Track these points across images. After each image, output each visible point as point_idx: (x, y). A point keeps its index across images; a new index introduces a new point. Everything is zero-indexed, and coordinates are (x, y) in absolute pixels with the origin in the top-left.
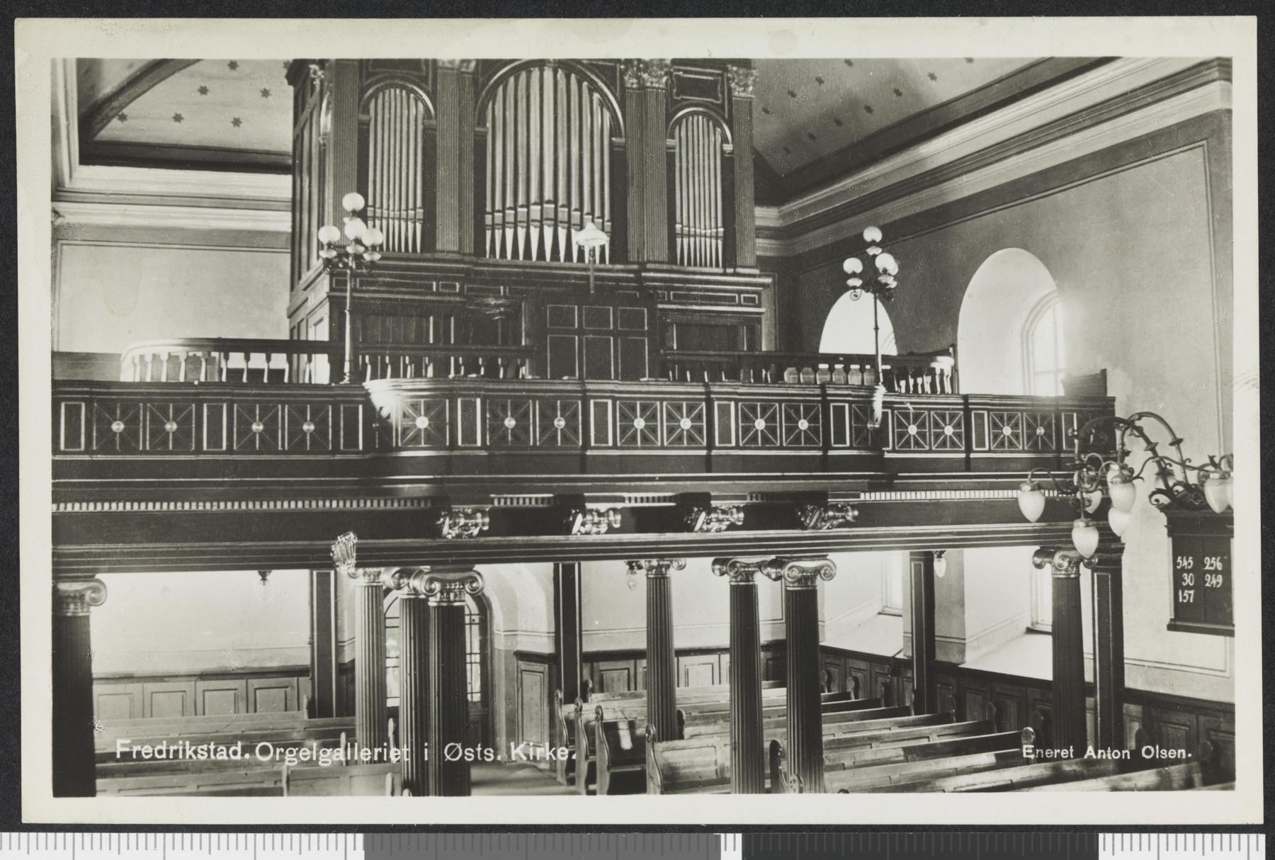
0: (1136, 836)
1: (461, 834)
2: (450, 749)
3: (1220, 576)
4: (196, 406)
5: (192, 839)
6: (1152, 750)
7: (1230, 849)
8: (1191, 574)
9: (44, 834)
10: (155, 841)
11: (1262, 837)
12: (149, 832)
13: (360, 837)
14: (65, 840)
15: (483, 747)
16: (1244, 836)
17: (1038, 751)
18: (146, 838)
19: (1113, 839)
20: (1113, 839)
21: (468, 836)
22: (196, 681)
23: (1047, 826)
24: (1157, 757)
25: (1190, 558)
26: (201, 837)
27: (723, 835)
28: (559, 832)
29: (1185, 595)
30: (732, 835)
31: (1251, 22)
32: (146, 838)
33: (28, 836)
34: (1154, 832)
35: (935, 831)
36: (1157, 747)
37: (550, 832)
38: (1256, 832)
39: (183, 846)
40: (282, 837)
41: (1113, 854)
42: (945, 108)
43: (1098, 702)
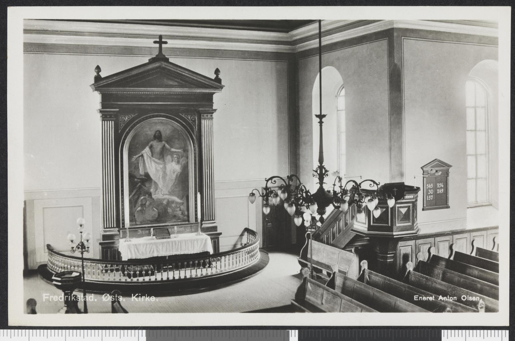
0: (457, 331)
1: (185, 330)
3: (442, 189)
5: (487, 332)
8: (432, 190)
9: (17, 330)
11: (507, 331)
12: (59, 329)
13: (144, 331)
14: (14, 332)
16: (500, 331)
18: (469, 332)
19: (142, 333)
20: (142, 333)
21: (188, 331)
22: (191, 270)
23: (421, 327)
24: (468, 300)
25: (432, 184)
26: (80, 331)
27: (290, 331)
28: (225, 329)
29: (430, 197)
30: (294, 330)
32: (469, 332)
33: (91, 331)
35: (376, 329)
36: (468, 296)
37: (221, 329)
38: (505, 330)
40: (80, 331)
43: (193, 135)
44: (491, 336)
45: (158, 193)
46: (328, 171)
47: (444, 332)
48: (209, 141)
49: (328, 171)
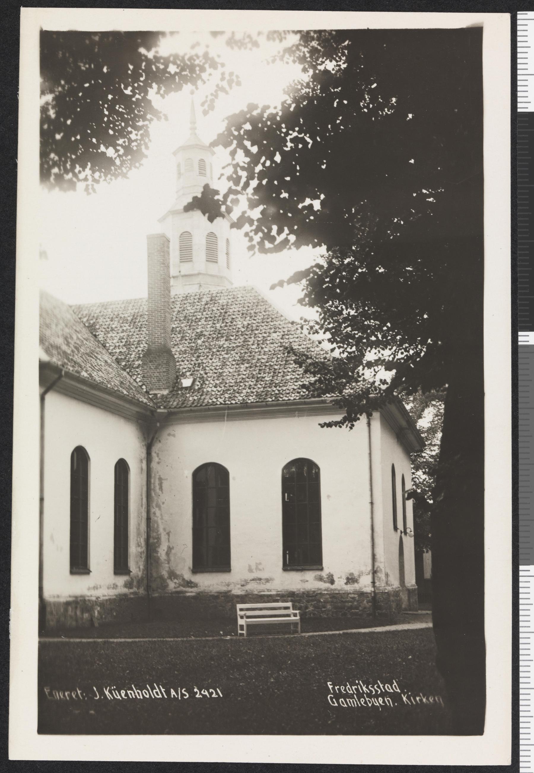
4: (287, 495)
13: (521, 568)
31: (23, 10)
41: (530, 47)
42: (48, 616)
44: (530, 683)
45: (285, 59)
46: (250, 566)
47: (521, 108)
48: (185, 255)
49: (250, 566)
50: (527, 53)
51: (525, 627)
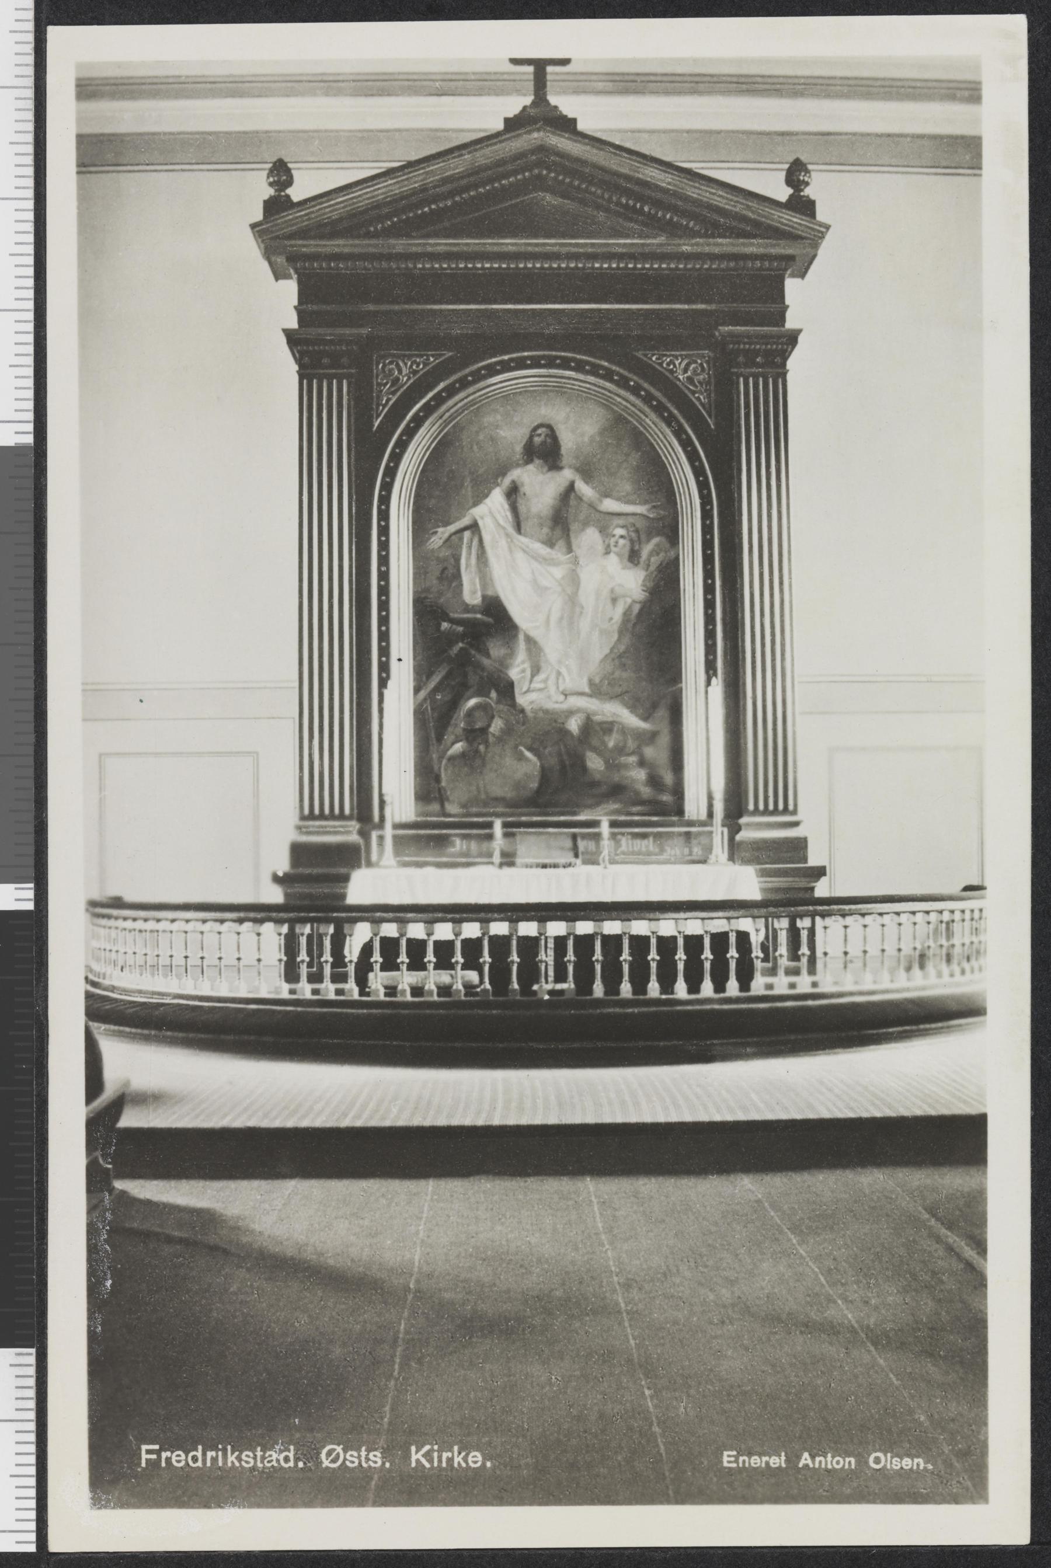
2: (329, 1453)
5: (26, 344)
6: (883, 1459)
7: (17, 900)
10: (24, 210)
11: (32, 1548)
13: (29, 439)
15: (368, 1451)
17: (741, 1459)
19: (25, 321)
31: (1017, 24)
32: (28, 210)
34: (37, 1393)
39: (20, 388)
41: (11, 255)
47: (28, 1356)
50: (17, 1498)
51: (22, 255)
